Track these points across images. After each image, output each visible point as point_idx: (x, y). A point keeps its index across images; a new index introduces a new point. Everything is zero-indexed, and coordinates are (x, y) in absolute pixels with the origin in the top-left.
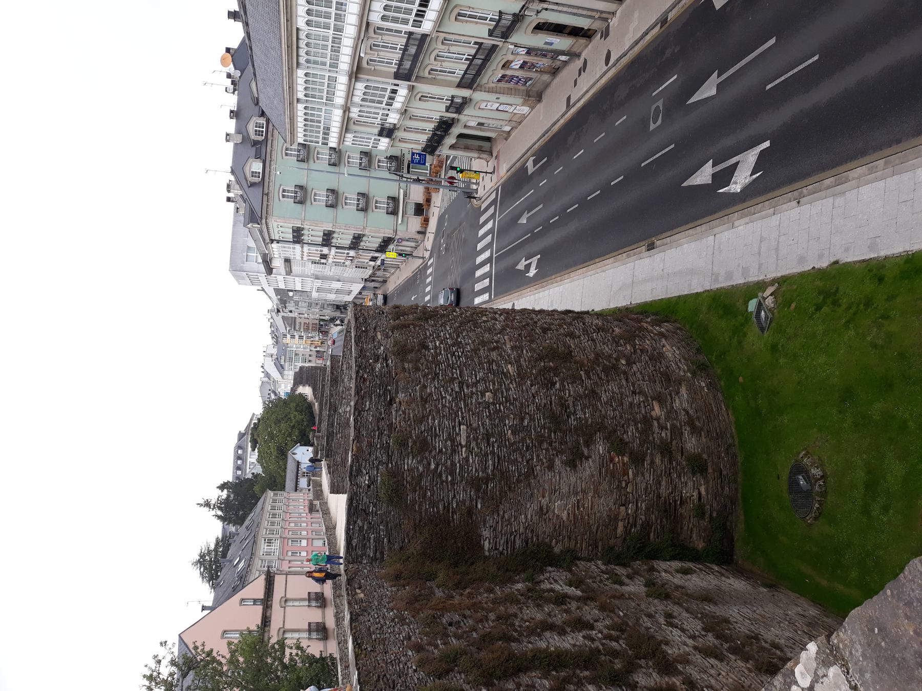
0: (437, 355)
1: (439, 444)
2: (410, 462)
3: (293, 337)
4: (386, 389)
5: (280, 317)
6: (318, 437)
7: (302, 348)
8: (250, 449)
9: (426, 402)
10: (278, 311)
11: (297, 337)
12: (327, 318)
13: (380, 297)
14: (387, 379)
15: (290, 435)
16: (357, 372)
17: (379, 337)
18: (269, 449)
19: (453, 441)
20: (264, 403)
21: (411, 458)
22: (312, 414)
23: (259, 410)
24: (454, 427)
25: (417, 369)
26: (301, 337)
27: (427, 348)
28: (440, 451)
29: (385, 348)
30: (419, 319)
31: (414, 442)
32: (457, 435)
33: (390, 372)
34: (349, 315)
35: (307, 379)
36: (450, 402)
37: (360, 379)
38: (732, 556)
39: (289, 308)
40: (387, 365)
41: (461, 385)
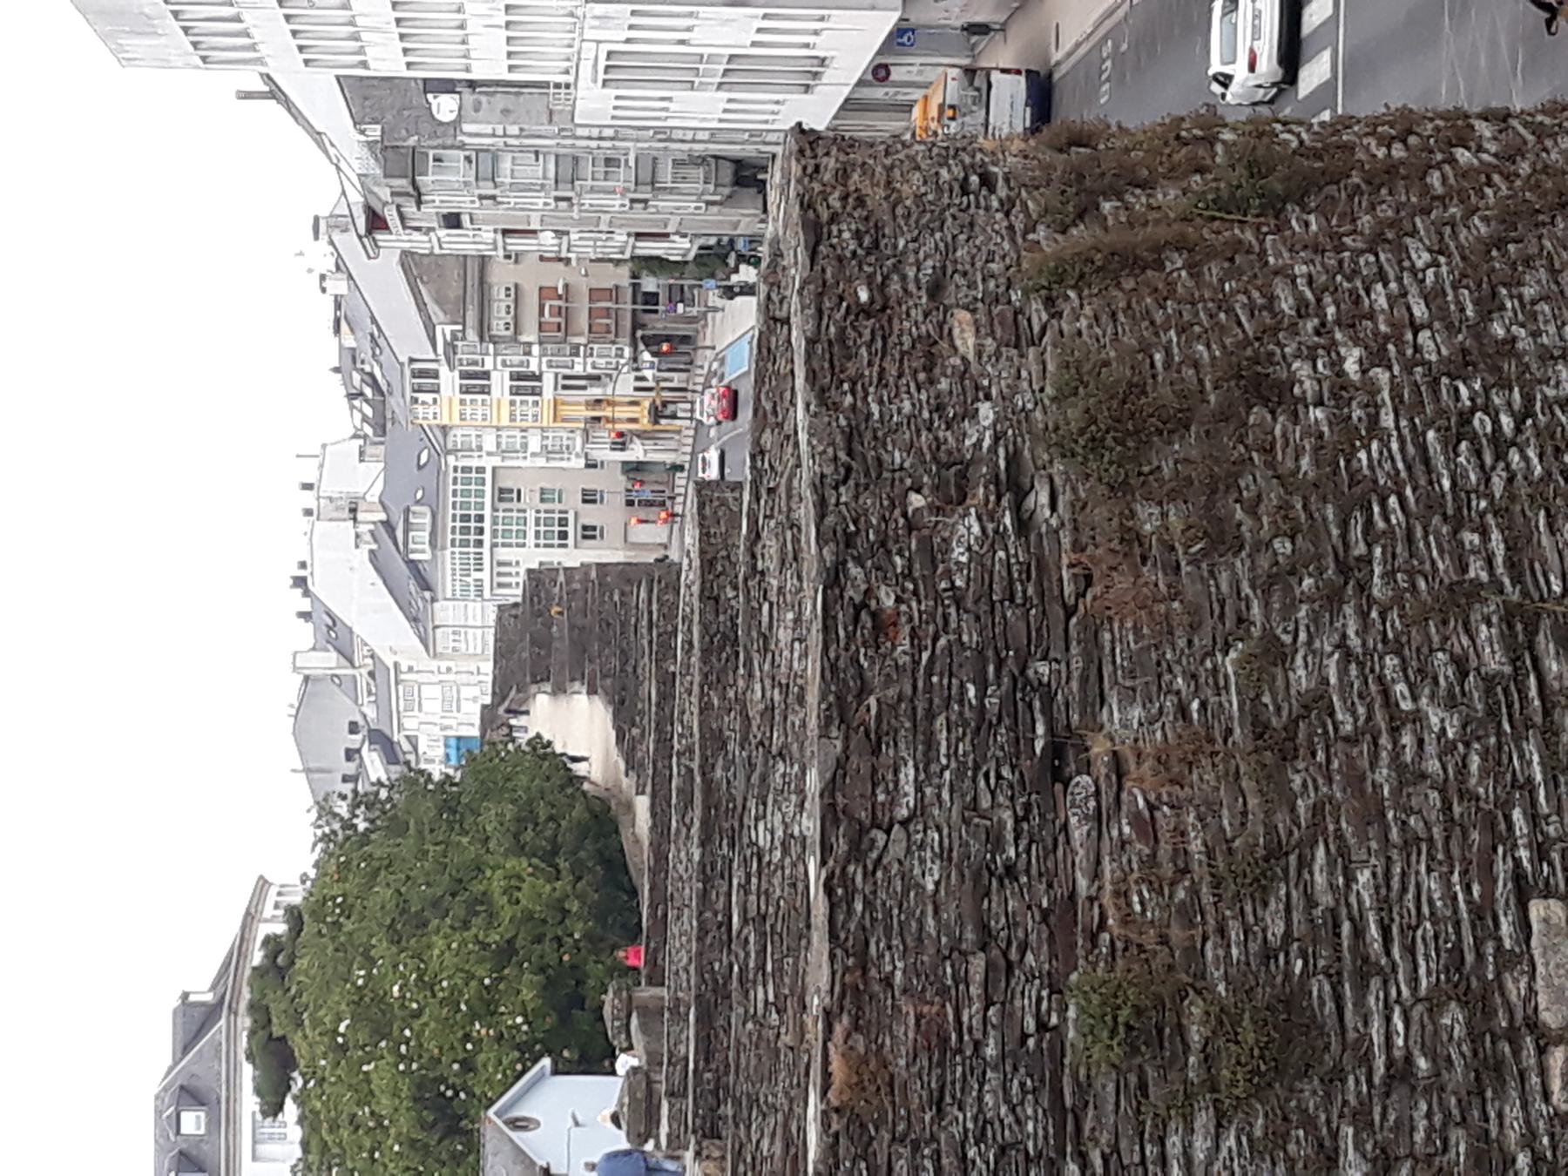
0: (1349, 437)
1: (1386, 1030)
2: (1201, 1146)
3: (475, 382)
4: (1021, 681)
5: (390, 260)
6: (651, 1014)
7: (558, 465)
8: (250, 1104)
9: (1287, 756)
10: (376, 222)
11: (500, 382)
12: (679, 248)
13: (1009, 94)
14: (1026, 615)
15: (487, 1008)
16: (834, 579)
17: (966, 341)
18: (368, 1097)
19: (1480, 1003)
20: (324, 810)
21: (1204, 1119)
22: (615, 865)
23: (291, 857)
24: (1483, 913)
25: (1220, 540)
26: (525, 383)
27: (1280, 395)
28: (1400, 1072)
29: (1012, 417)
30: (1227, 206)
31: (1223, 1022)
32: (1507, 960)
33: (1040, 568)
34: (776, 220)
35: (580, 649)
36: (1447, 748)
37: (852, 622)
38: (575, 780)
39: (438, 202)
40: (1024, 524)
41: (1520, 624)
